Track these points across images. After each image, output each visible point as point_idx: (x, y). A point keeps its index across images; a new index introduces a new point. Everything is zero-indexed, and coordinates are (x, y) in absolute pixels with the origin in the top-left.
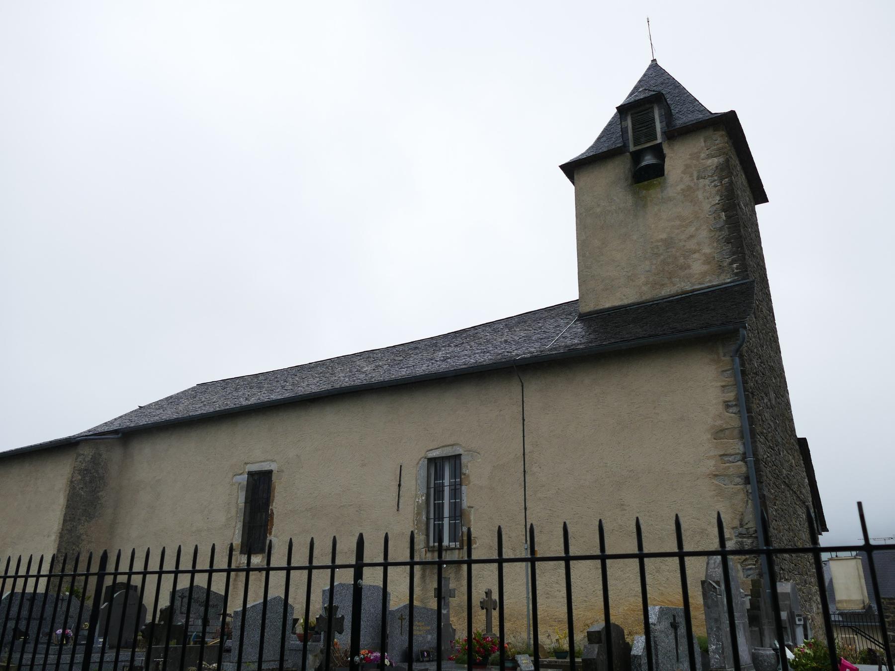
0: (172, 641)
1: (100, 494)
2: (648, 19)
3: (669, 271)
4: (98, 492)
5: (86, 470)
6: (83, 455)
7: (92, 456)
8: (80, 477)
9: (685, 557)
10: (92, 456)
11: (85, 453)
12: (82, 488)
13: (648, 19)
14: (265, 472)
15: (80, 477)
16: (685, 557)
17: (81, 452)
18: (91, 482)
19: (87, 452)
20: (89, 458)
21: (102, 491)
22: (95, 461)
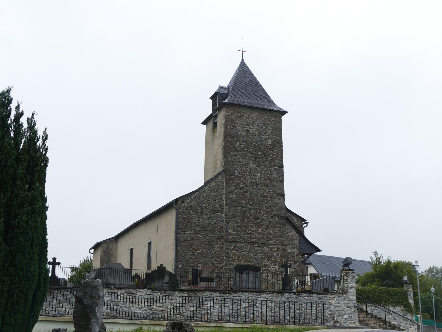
0: (225, 108)
1: (111, 258)
2: (242, 38)
3: (399, 319)
4: (110, 258)
5: (105, 251)
6: (103, 247)
7: (10, 281)
8: (103, 254)
9: (52, 261)
10: (10, 281)
11: (104, 246)
12: (104, 257)
13: (242, 38)
14: (235, 82)
15: (103, 254)
16: (52, 261)
17: (102, 246)
18: (107, 255)
19: (104, 246)
20: (105, 248)
21: (111, 257)
22: (107, 248)
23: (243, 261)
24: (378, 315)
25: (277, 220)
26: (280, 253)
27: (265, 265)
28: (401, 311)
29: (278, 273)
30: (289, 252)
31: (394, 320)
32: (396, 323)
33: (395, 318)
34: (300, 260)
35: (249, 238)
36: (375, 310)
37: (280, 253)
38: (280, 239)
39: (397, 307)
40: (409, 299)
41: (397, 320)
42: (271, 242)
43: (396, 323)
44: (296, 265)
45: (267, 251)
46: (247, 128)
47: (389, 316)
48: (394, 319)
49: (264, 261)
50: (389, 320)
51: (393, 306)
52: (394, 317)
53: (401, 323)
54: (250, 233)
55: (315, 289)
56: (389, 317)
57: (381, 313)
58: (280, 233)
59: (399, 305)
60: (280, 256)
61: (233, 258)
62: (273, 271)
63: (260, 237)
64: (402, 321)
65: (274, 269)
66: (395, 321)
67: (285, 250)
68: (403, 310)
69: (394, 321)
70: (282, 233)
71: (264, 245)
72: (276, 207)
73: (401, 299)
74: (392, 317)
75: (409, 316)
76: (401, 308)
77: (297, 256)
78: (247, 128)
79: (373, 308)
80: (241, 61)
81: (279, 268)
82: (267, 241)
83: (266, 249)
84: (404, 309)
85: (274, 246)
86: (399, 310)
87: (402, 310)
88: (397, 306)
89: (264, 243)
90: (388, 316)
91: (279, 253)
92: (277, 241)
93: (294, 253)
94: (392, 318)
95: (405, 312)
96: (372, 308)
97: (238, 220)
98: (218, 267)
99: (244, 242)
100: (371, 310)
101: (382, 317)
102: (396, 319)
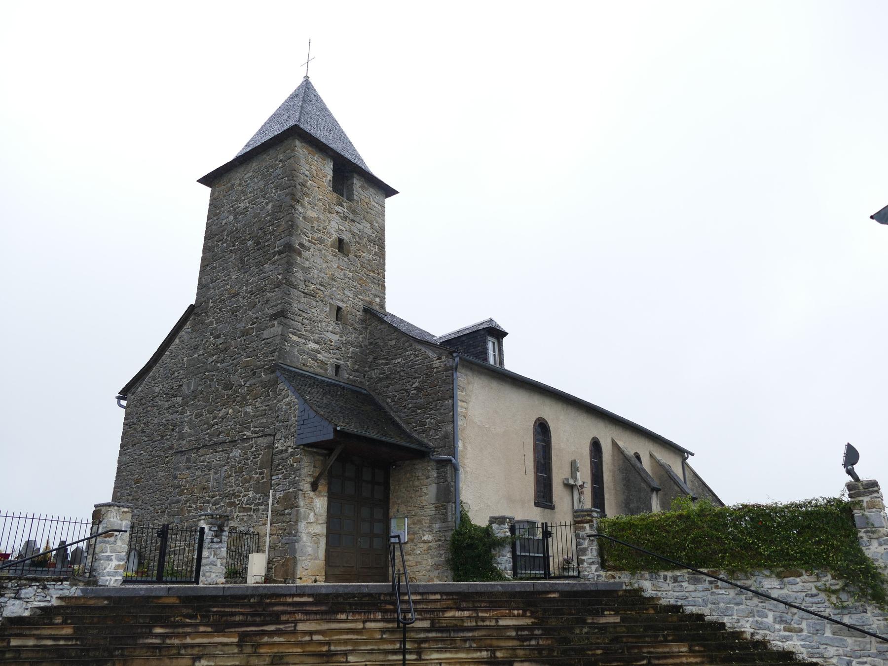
23: (196, 490)
24: (706, 611)
25: (264, 376)
26: (260, 456)
27: (231, 492)
28: (823, 596)
29: (251, 508)
30: (277, 450)
31: (787, 633)
32: (803, 646)
33: (796, 626)
34: (297, 465)
35: (211, 435)
36: (693, 594)
37: (260, 456)
38: (262, 423)
39: (798, 580)
40: (865, 538)
41: (805, 633)
42: (247, 434)
43: (803, 646)
44: (287, 480)
45: (237, 457)
46: (236, 206)
47: (762, 617)
48: (785, 630)
49: (229, 482)
50: (761, 632)
51: (779, 576)
52: (786, 622)
53: (829, 648)
54: (215, 424)
55: (563, 528)
56: (764, 619)
57: (722, 605)
58: (266, 406)
59: (810, 571)
60: (261, 463)
61: (182, 487)
62: (244, 506)
63: (229, 427)
64: (831, 639)
65: (246, 498)
66: (795, 638)
67: (271, 446)
68: (834, 592)
69: (787, 639)
70: (268, 405)
71: (234, 444)
72: (263, 348)
73: (819, 543)
74: (775, 622)
75: (869, 614)
76: (819, 584)
77: (292, 455)
78: (236, 206)
79: (685, 584)
80: (302, 80)
81: (254, 494)
82: (240, 434)
83: (236, 452)
84: (840, 584)
85: (252, 441)
86: (814, 591)
87: (829, 591)
88: (802, 575)
89: (234, 439)
90: (757, 618)
91: (257, 458)
92: (257, 429)
93: (286, 450)
94: (777, 626)
95: (844, 596)
96: (681, 586)
97: (199, 401)
98: (158, 513)
99: (204, 446)
100: (677, 594)
101: (726, 620)
102: (801, 630)
